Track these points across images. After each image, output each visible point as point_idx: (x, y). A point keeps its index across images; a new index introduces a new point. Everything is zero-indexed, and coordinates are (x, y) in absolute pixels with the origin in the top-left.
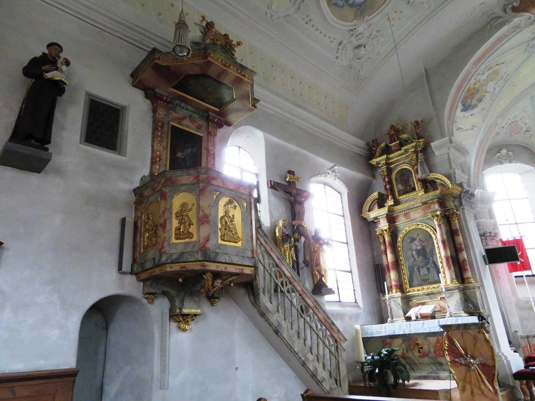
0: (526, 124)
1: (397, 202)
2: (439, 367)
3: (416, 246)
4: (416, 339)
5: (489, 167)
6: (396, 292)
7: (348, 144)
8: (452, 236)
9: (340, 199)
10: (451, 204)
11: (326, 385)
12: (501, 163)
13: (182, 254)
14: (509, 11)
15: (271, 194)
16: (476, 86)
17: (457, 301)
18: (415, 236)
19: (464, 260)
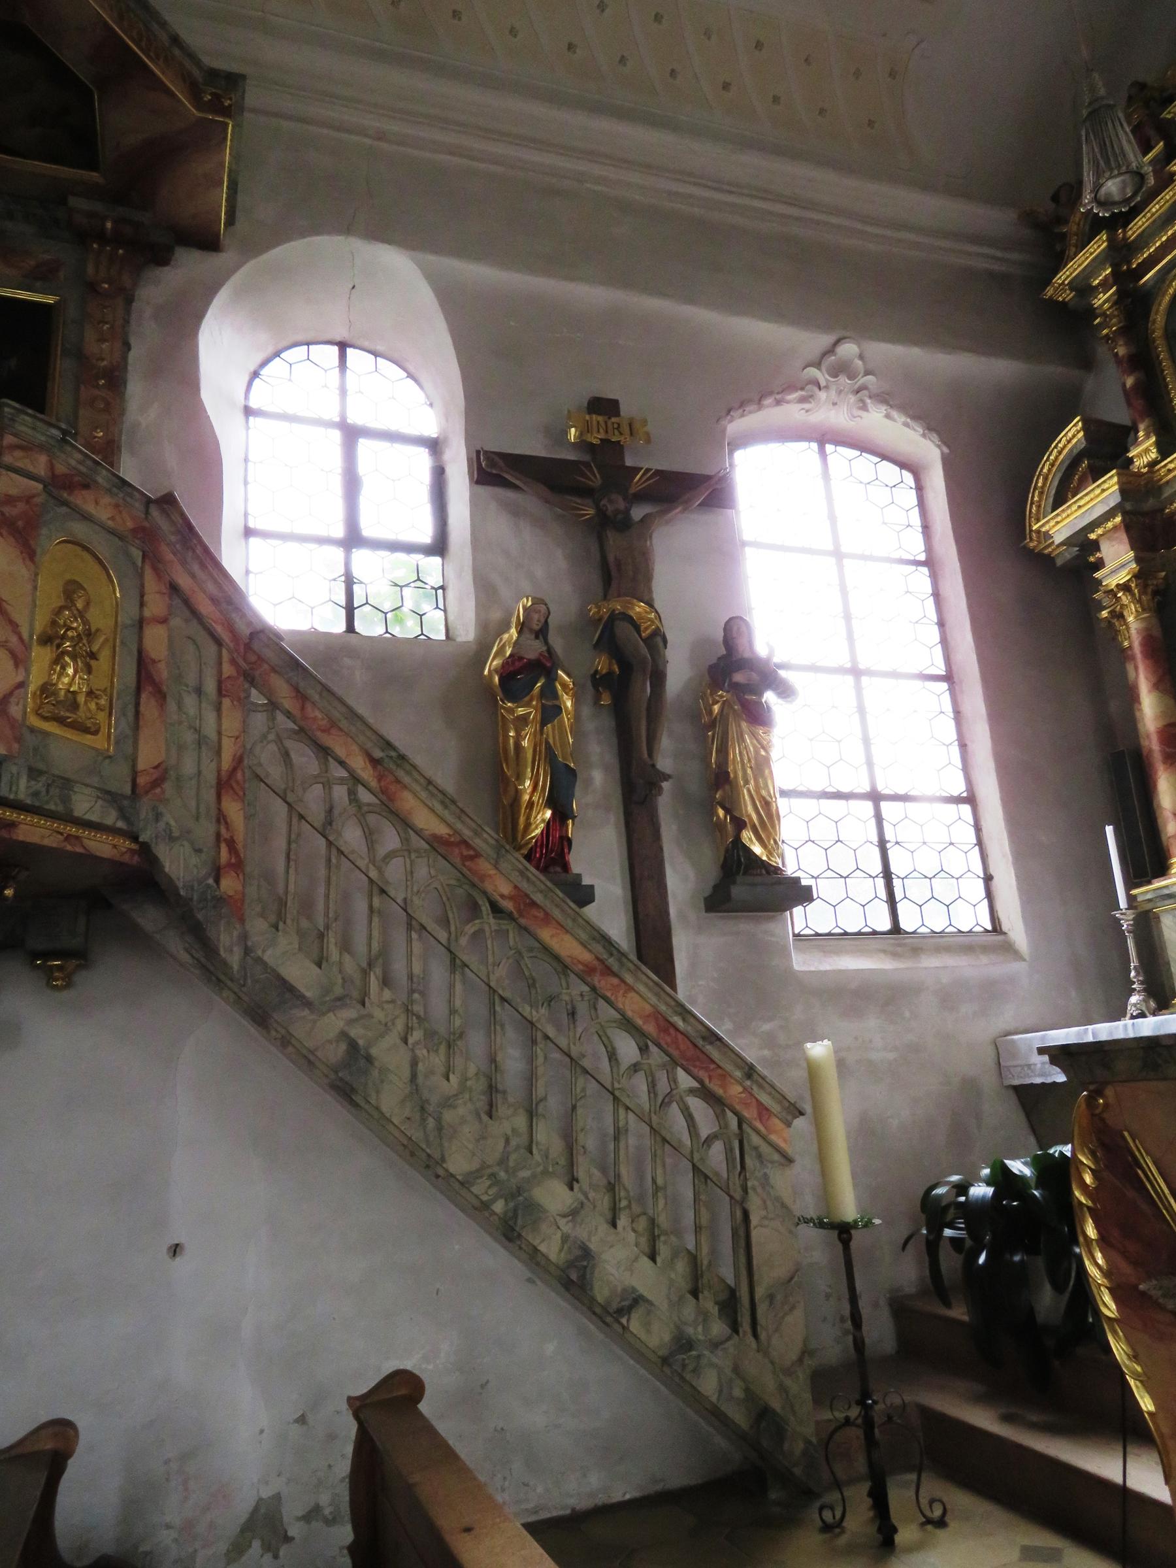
7: (912, 237)
11: (647, 1325)
15: (493, 506)
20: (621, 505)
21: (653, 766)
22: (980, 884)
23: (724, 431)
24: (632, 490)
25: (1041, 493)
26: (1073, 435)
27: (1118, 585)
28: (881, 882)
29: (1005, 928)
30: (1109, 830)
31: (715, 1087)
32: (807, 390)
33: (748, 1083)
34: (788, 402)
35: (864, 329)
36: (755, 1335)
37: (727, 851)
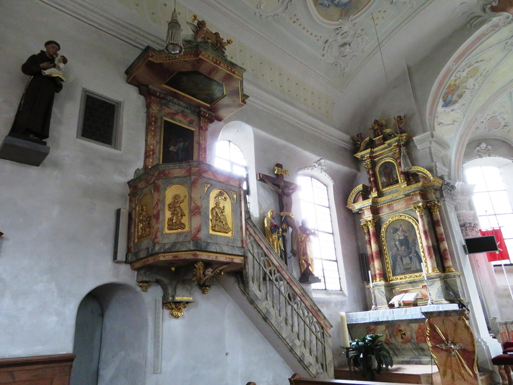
0: (504, 119)
1: (381, 194)
2: (421, 353)
3: (399, 237)
4: (399, 326)
5: (469, 161)
6: (380, 281)
7: (333, 138)
8: (434, 226)
9: (326, 191)
10: (432, 196)
11: (312, 369)
12: (480, 157)
13: (174, 244)
14: (488, 10)
15: (260, 186)
16: (457, 83)
17: (438, 289)
18: (398, 226)
19: (445, 250)
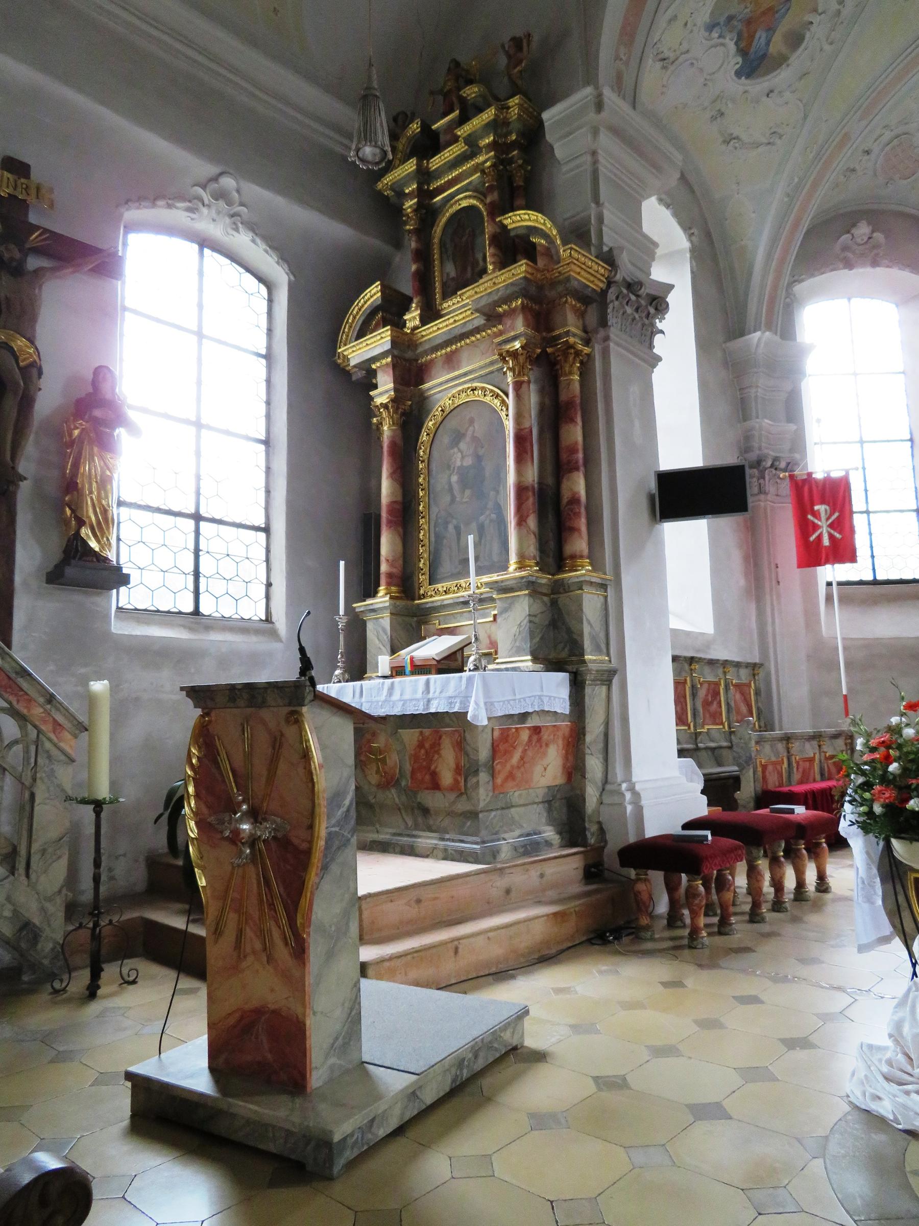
2: (420, 820)
3: (463, 458)
9: (265, 304)
10: (570, 327)
12: (849, 265)
17: (520, 625)
19: (575, 500)
20: (17, 255)
21: (13, 468)
22: (263, 588)
23: (121, 215)
24: (27, 246)
25: (350, 327)
26: (373, 294)
27: (381, 404)
28: (191, 579)
29: (274, 619)
30: (342, 563)
31: (21, 708)
32: (194, 204)
33: (49, 706)
34: (177, 208)
35: (242, 171)
36: (28, 876)
37: (69, 541)
